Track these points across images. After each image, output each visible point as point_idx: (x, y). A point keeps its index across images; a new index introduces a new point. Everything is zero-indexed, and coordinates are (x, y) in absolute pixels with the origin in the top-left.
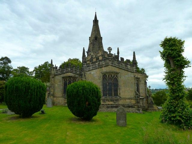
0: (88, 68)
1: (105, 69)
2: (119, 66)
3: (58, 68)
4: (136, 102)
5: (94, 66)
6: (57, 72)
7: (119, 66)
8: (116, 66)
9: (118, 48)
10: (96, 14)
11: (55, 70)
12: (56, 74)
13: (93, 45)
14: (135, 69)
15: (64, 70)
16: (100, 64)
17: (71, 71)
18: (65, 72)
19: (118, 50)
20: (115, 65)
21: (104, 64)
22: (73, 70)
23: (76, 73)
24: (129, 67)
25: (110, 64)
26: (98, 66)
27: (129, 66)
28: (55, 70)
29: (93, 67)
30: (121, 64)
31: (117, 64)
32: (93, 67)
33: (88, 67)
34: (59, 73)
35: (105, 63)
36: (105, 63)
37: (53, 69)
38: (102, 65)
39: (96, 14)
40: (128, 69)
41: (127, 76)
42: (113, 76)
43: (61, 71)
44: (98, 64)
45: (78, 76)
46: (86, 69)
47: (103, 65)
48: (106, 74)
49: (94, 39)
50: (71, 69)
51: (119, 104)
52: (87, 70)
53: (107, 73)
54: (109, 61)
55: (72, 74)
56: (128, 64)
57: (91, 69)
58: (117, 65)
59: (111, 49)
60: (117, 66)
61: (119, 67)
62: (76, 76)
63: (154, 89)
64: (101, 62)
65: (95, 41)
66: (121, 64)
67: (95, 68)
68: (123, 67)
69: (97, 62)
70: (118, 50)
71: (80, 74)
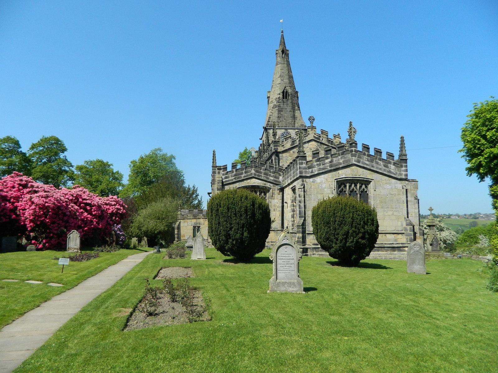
0: (310, 170)
1: (344, 174)
2: (373, 167)
3: (20, 150)
4: (407, 238)
5: (322, 167)
6: (226, 178)
7: (373, 167)
8: (365, 166)
10: (283, 37)
11: (222, 173)
12: (226, 181)
13: (280, 111)
15: (242, 174)
16: (334, 162)
18: (244, 177)
21: (341, 161)
22: (261, 173)
23: (268, 179)
26: (331, 166)
27: (392, 167)
28: (222, 173)
30: (377, 163)
31: (367, 163)
32: (320, 169)
33: (309, 168)
34: (230, 179)
35: (343, 160)
36: (343, 160)
37: (217, 171)
38: (337, 165)
39: (283, 37)
40: (390, 172)
41: (388, 187)
43: (235, 175)
44: (331, 162)
45: (272, 185)
46: (306, 172)
49: (281, 96)
50: (257, 171)
52: (308, 175)
54: (353, 155)
55: (260, 181)
56: (390, 163)
57: (316, 173)
58: (367, 165)
59: (314, 119)
60: (368, 167)
61: (372, 168)
62: (268, 185)
63: (79, 236)
64: (334, 159)
65: (284, 102)
66: (377, 163)
67: (324, 171)
68: (380, 169)
69: (327, 158)
71: (275, 181)
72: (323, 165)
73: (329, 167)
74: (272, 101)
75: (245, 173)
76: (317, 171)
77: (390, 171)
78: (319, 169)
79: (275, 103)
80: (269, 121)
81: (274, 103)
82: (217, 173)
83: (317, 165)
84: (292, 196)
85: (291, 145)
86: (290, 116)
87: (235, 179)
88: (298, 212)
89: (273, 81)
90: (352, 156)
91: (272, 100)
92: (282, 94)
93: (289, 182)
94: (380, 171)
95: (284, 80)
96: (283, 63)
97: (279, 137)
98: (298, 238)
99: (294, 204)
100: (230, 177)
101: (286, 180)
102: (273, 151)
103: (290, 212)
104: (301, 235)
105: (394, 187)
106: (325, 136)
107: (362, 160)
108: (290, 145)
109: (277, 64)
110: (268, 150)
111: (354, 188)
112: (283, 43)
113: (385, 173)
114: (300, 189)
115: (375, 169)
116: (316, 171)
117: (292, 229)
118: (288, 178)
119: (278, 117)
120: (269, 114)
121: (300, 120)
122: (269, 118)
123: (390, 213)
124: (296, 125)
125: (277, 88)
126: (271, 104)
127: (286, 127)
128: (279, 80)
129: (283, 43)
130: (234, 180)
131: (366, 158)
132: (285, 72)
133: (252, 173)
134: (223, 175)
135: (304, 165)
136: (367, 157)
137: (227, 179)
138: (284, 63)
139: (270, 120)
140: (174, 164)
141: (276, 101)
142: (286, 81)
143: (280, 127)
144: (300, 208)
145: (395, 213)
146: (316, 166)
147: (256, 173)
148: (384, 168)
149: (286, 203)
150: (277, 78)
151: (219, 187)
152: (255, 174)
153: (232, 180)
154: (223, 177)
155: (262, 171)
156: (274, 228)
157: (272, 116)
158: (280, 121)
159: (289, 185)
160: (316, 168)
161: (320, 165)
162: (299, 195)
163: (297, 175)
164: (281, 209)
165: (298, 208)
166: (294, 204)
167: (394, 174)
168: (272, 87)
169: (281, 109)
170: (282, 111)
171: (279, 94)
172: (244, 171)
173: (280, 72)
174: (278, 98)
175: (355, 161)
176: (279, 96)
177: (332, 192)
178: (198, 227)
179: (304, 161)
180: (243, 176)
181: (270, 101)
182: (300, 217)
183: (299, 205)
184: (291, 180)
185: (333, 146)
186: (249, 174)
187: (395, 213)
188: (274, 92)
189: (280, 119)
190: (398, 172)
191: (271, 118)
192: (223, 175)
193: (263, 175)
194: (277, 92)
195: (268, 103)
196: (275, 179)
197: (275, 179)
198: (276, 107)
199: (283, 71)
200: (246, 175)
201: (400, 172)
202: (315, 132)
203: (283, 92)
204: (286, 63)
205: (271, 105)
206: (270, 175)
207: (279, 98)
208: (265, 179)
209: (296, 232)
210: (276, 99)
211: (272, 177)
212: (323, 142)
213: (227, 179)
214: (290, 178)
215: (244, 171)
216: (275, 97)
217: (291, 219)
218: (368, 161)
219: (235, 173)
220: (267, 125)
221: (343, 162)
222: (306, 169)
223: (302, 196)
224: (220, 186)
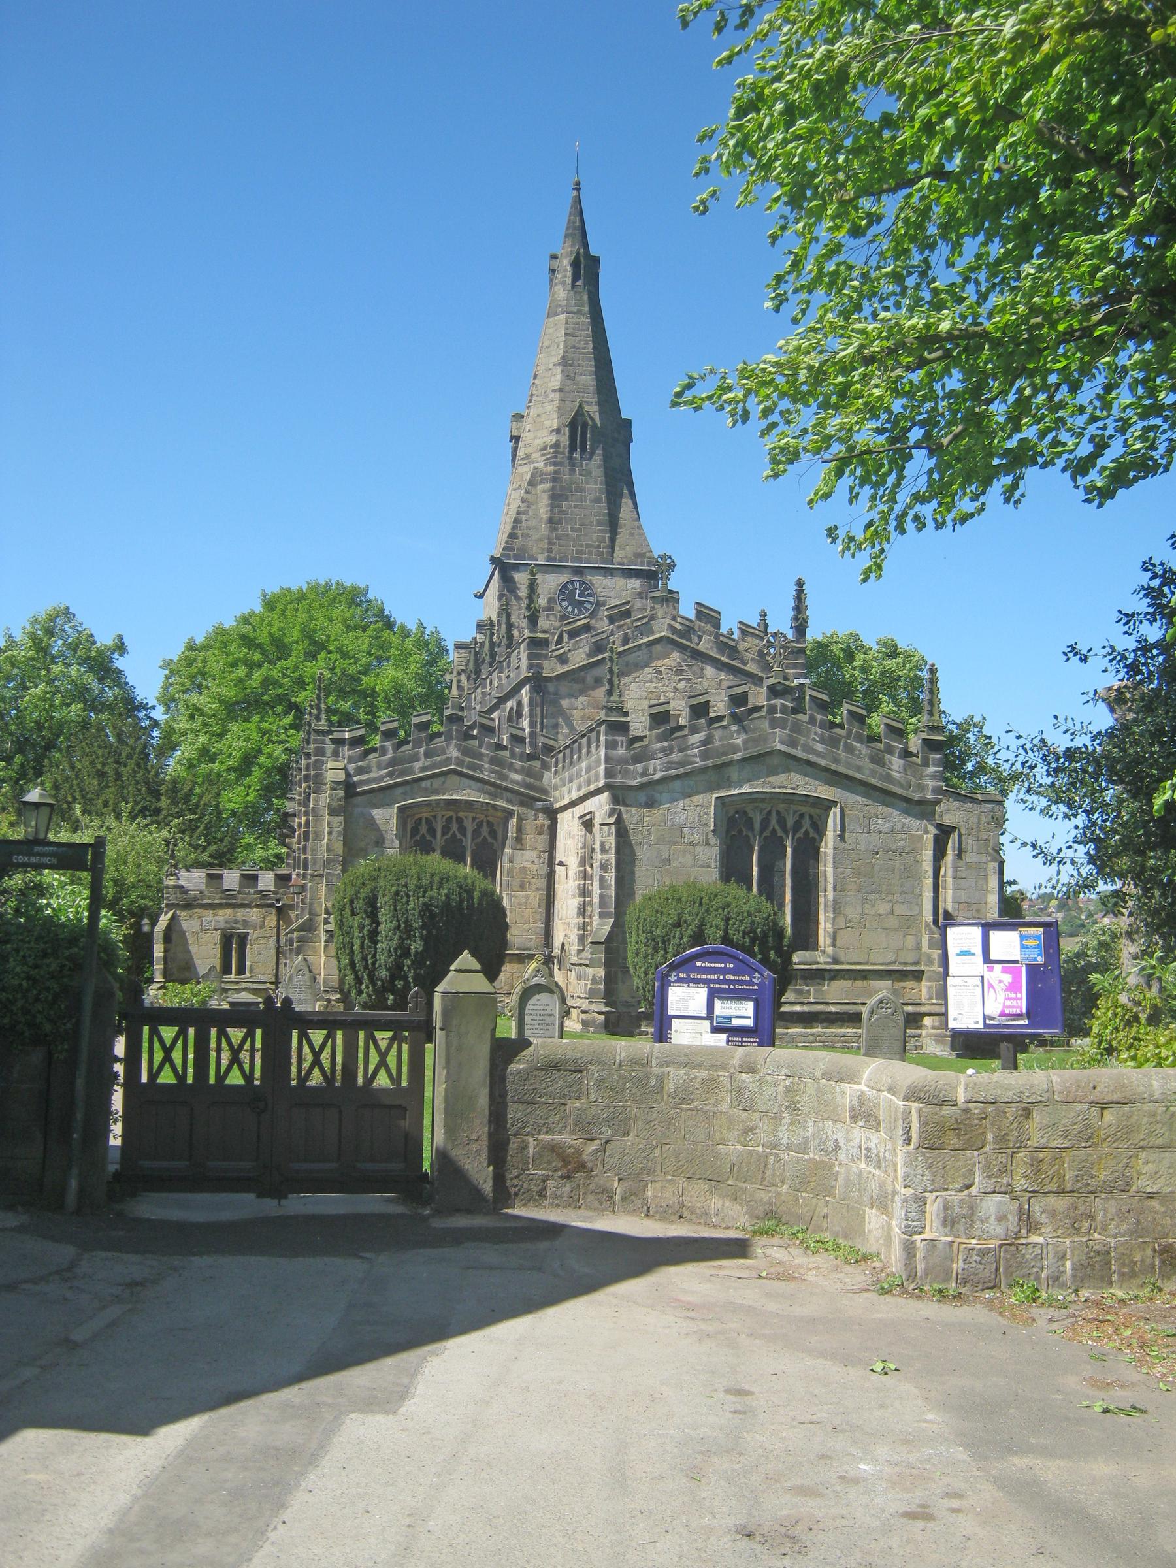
0: (640, 767)
5: (676, 757)
6: (360, 770)
7: (836, 760)
8: (813, 758)
9: (800, 583)
10: (578, 201)
13: (556, 497)
14: (932, 784)
15: (415, 758)
16: (717, 743)
17: (460, 762)
18: (423, 769)
19: (800, 595)
20: (808, 749)
22: (480, 756)
23: (504, 777)
24: (895, 767)
25: (781, 747)
26: (704, 756)
29: (669, 766)
30: (849, 749)
31: (819, 747)
32: (669, 766)
33: (637, 759)
34: (373, 775)
38: (724, 754)
39: (578, 201)
40: (888, 778)
41: (881, 825)
42: (790, 822)
43: (393, 763)
44: (705, 743)
46: (626, 774)
47: (735, 749)
48: (749, 809)
49: (565, 440)
50: (466, 752)
51: (827, 1003)
52: (633, 783)
53: (755, 801)
54: (774, 723)
57: (657, 776)
58: (818, 754)
61: (833, 767)
65: (573, 465)
66: (849, 749)
67: (682, 770)
68: (859, 769)
69: (694, 730)
70: (800, 595)
72: (680, 751)
73: (697, 759)
74: (528, 457)
75: (427, 755)
76: (661, 771)
77: (889, 775)
78: (668, 763)
79: (540, 465)
80: (512, 536)
81: (537, 465)
82: (329, 752)
83: (663, 750)
84: (580, 845)
85: (589, 656)
86: (594, 519)
87: (390, 775)
88: (596, 899)
89: (535, 377)
90: (772, 727)
91: (529, 450)
92: (567, 429)
93: (575, 795)
94: (858, 775)
95: (578, 378)
96: (575, 309)
97: (550, 600)
98: (594, 981)
99: (588, 869)
100: (374, 769)
101: (565, 789)
102: (525, 673)
103: (573, 896)
104: (601, 973)
105: (898, 827)
106: (709, 627)
107: (802, 739)
108: (584, 656)
109: (552, 313)
110: (509, 665)
111: (777, 827)
112: (579, 231)
113: (872, 781)
114: (606, 828)
115: (843, 770)
116: (657, 769)
117: (579, 952)
118: (571, 781)
119: (550, 520)
120: (514, 506)
121: (632, 535)
122: (516, 521)
123: (883, 908)
124: (618, 554)
125: (549, 408)
126: (525, 469)
127: (579, 560)
128: (559, 377)
129: (579, 231)
130: (388, 782)
131: (816, 734)
132: (582, 344)
133: (449, 759)
134: (351, 760)
135: (621, 752)
136: (819, 731)
137: (363, 777)
138: (579, 312)
139: (519, 532)
140: (120, 672)
141: (543, 455)
142: (587, 380)
143: (554, 560)
144: (602, 887)
145: (900, 909)
146: (660, 755)
147: (462, 757)
148: (871, 766)
149: (561, 864)
150: (551, 366)
151: (336, 804)
152: (460, 762)
153: (381, 779)
154: (351, 768)
155: (483, 750)
156: (518, 949)
157: (526, 513)
158: (558, 538)
159: (573, 804)
160: (657, 762)
161: (671, 753)
162: (602, 845)
163: (597, 779)
164: (543, 883)
165: (596, 884)
166: (588, 869)
167: (901, 786)
168: (530, 401)
169: (562, 488)
170: (566, 499)
171: (558, 431)
172: (422, 750)
173: (562, 346)
174: (553, 446)
175: (781, 742)
176: (553, 438)
177: (707, 839)
178: (239, 935)
179: (620, 738)
180: (418, 765)
181: (521, 453)
182: (602, 915)
183: (602, 877)
184: (579, 789)
185: (734, 663)
186: (439, 758)
187: (900, 909)
188: (538, 420)
189: (556, 529)
190: (914, 781)
191: (524, 525)
192: (351, 760)
193: (486, 766)
194: (547, 423)
195: (513, 461)
196: (529, 780)
197: (529, 780)
198: (542, 482)
199: (572, 340)
200: (427, 762)
201: (920, 779)
202: (674, 613)
203: (573, 425)
204: (586, 309)
205: (526, 471)
206: (511, 767)
207: (556, 445)
208: (492, 778)
209: (587, 962)
210: (545, 448)
211: (517, 771)
212: (701, 647)
213: (363, 777)
214: (576, 782)
215: (422, 750)
216: (539, 442)
217: (576, 920)
218: (822, 741)
219: (390, 754)
220: (507, 548)
221: (745, 742)
222: (628, 763)
223: (610, 848)
224: (339, 800)
